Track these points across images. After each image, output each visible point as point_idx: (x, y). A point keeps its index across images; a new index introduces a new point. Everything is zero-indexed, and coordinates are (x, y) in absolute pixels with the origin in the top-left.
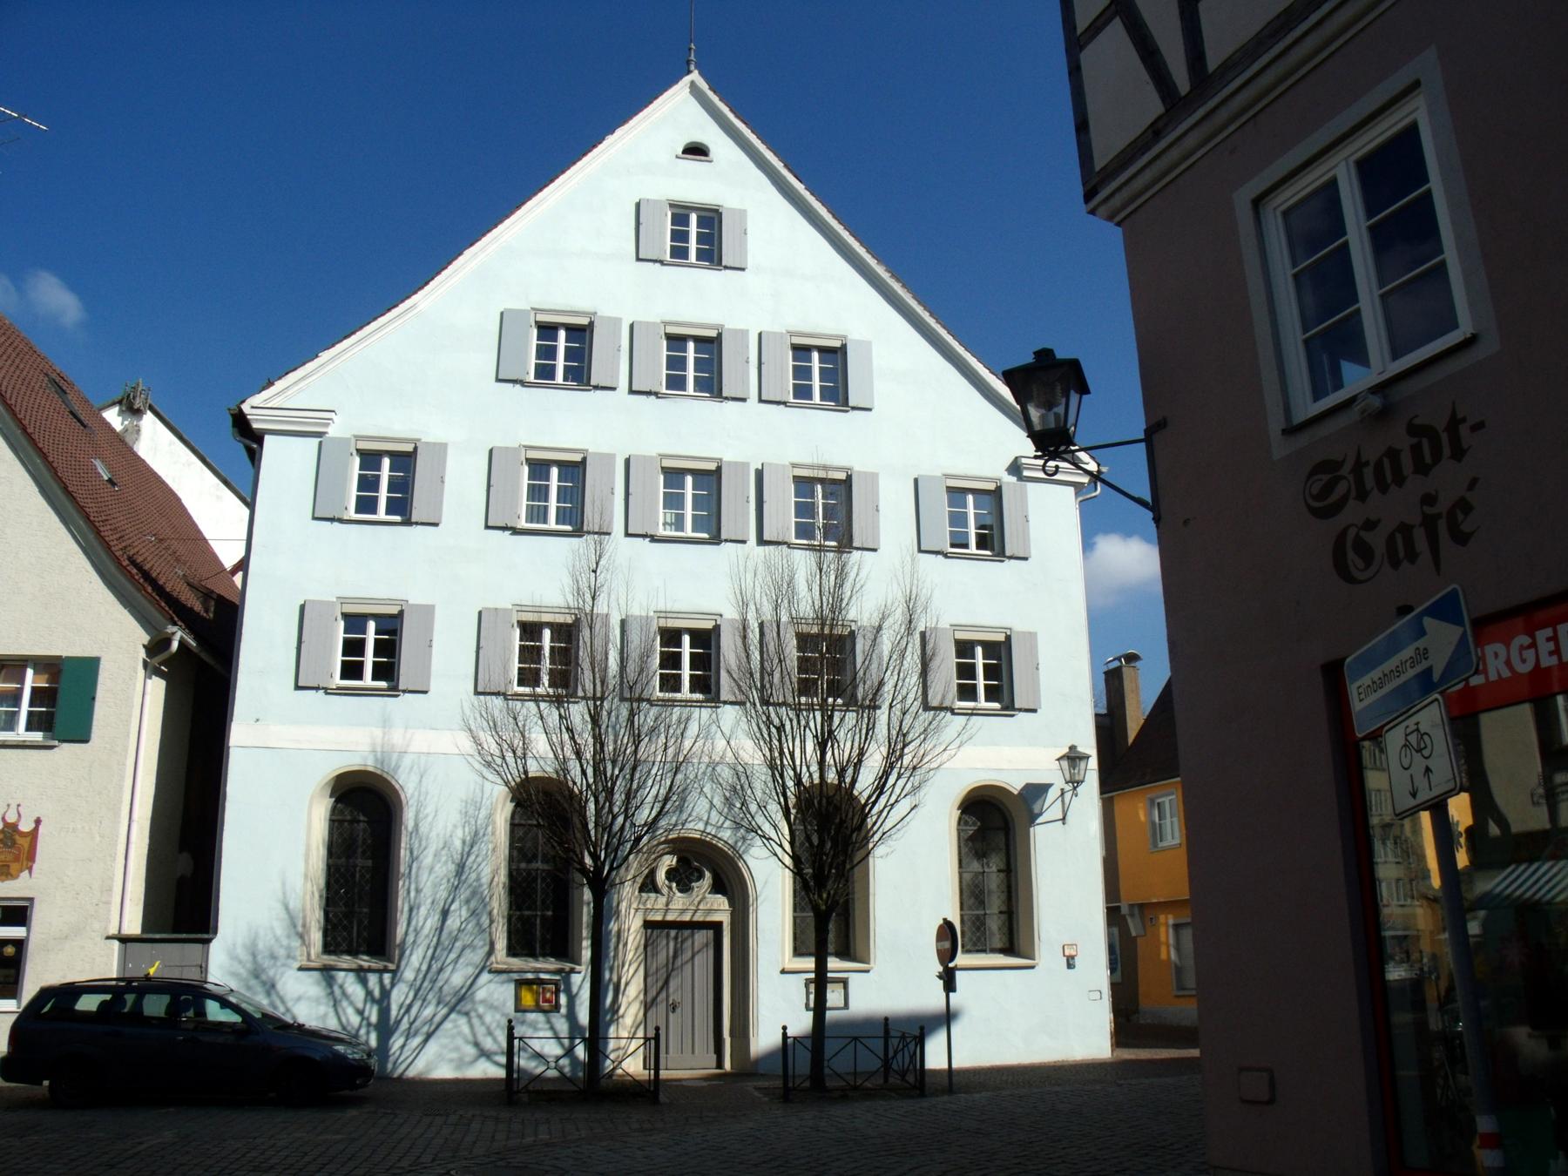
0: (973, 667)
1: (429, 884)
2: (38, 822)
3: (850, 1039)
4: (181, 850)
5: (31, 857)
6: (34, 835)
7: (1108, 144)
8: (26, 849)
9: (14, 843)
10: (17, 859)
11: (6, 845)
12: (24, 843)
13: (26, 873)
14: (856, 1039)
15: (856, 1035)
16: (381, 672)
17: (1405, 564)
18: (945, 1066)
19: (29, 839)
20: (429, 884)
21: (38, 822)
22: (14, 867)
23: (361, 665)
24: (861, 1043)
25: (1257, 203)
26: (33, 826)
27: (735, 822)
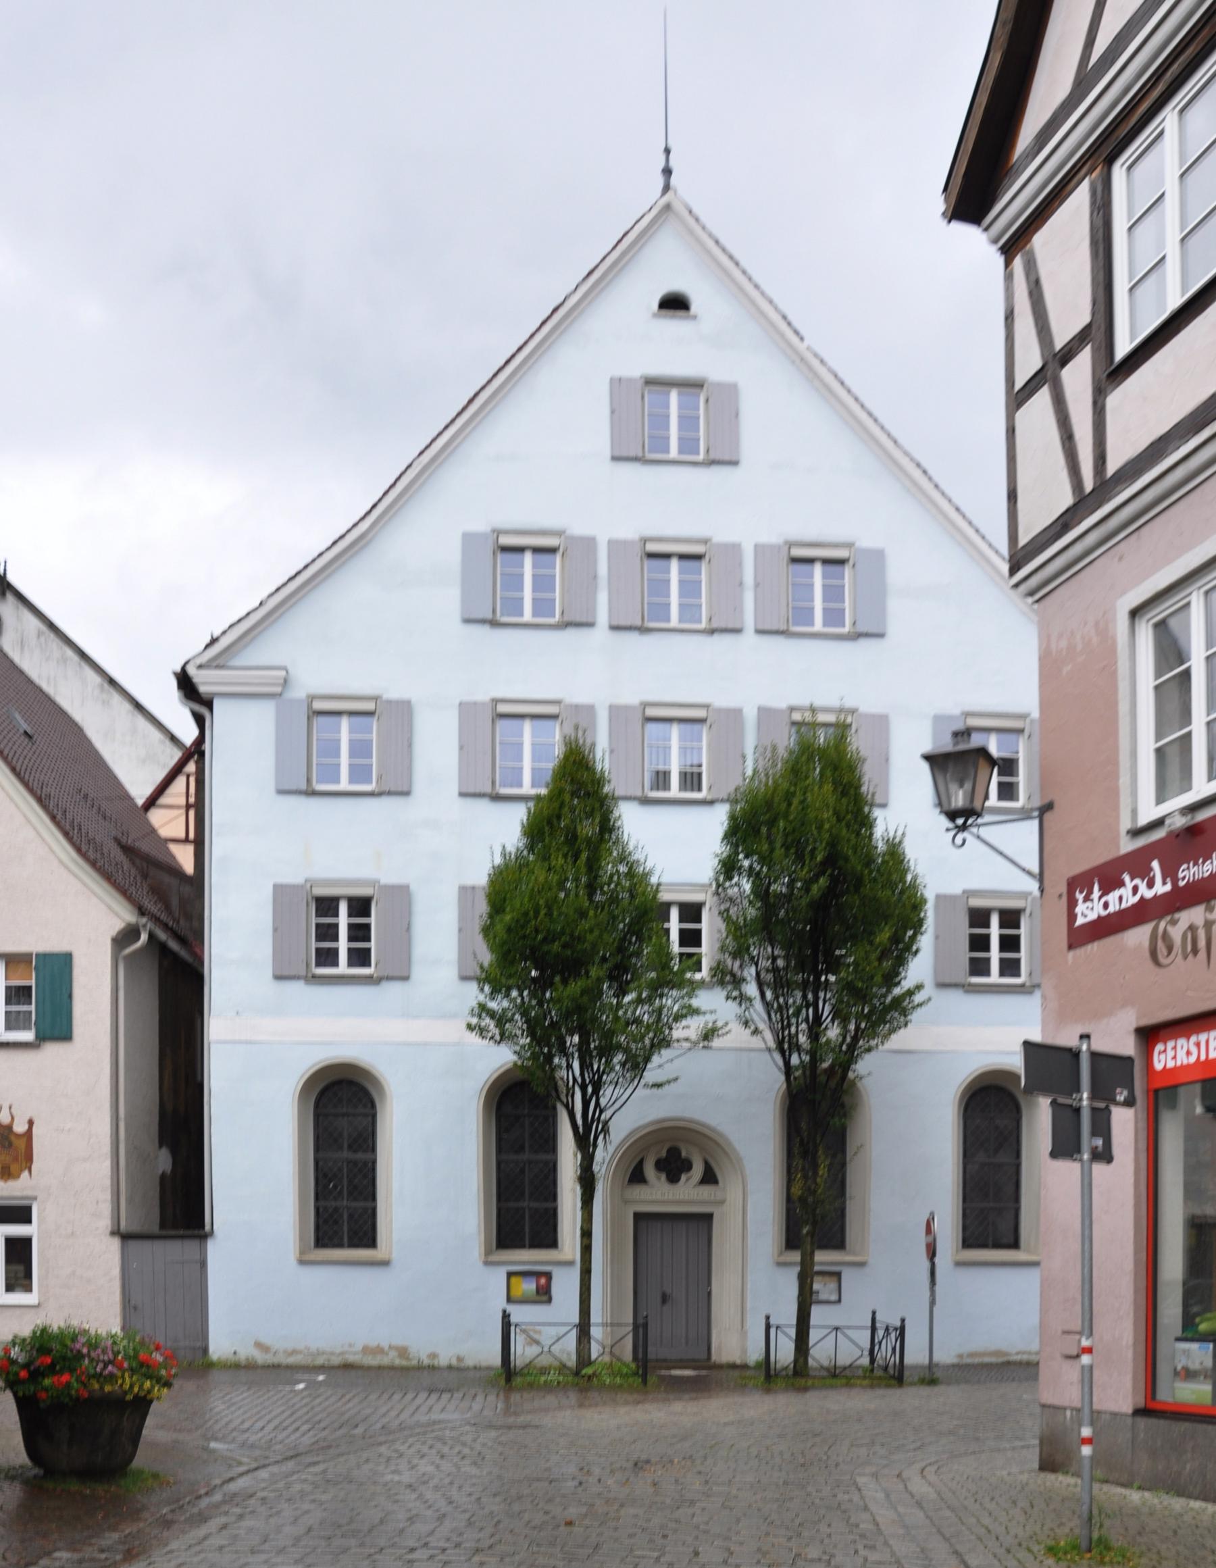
0: (986, 938)
1: (67, 825)
2: (31, 1123)
3: (826, 1331)
4: (161, 1146)
5: (29, 1158)
6: (29, 1134)
7: (1032, 525)
8: (23, 1151)
9: (10, 1145)
10: (16, 1159)
11: (4, 1146)
12: (22, 1144)
13: (25, 1174)
14: (837, 1329)
15: (837, 1324)
16: (360, 957)
17: (1190, 957)
18: (927, 1362)
19: (25, 1139)
20: (67, 825)
21: (31, 1123)
22: (14, 1168)
23: (335, 952)
24: (830, 1333)
25: (1135, 613)
26: (26, 1127)
27: (251, 1496)
